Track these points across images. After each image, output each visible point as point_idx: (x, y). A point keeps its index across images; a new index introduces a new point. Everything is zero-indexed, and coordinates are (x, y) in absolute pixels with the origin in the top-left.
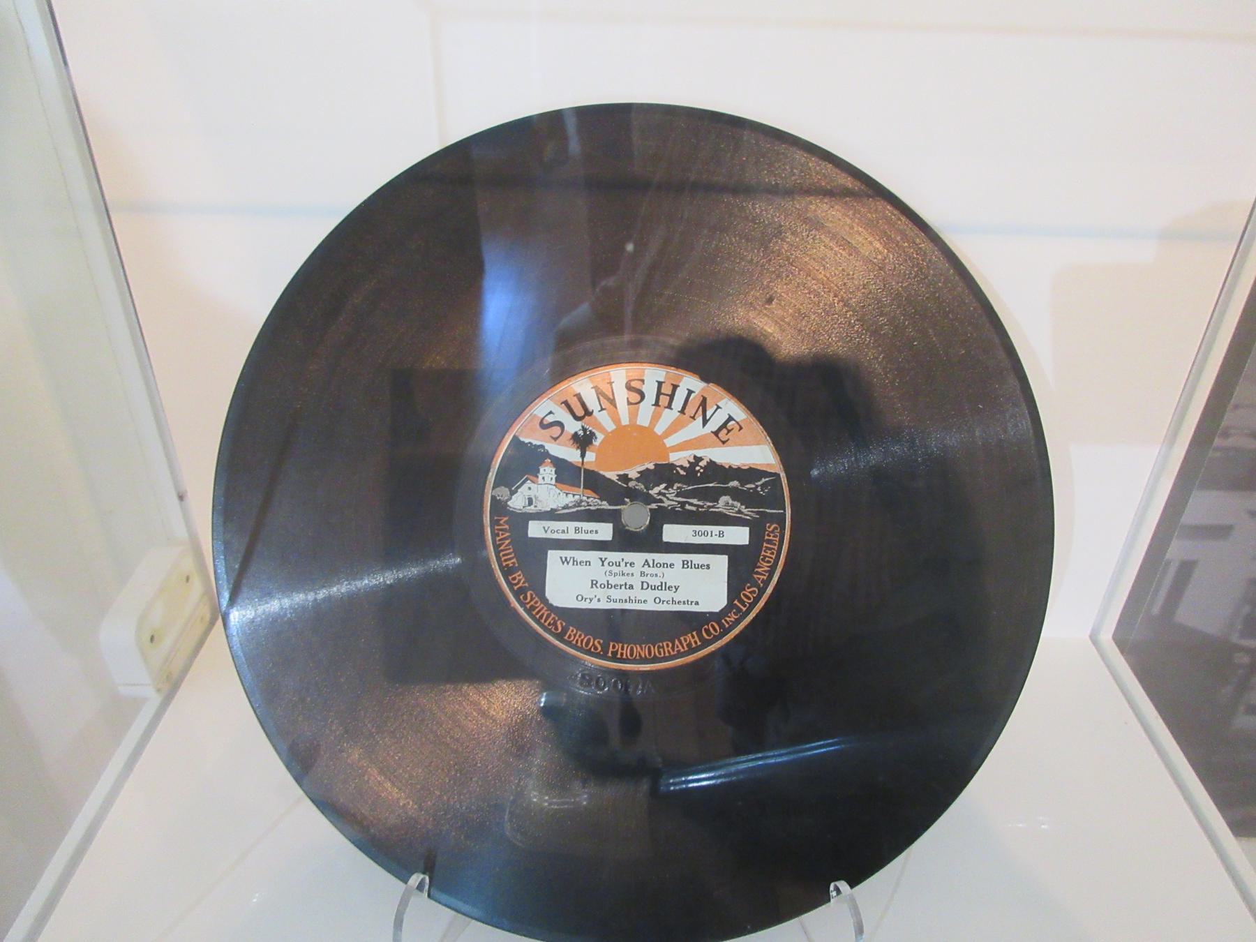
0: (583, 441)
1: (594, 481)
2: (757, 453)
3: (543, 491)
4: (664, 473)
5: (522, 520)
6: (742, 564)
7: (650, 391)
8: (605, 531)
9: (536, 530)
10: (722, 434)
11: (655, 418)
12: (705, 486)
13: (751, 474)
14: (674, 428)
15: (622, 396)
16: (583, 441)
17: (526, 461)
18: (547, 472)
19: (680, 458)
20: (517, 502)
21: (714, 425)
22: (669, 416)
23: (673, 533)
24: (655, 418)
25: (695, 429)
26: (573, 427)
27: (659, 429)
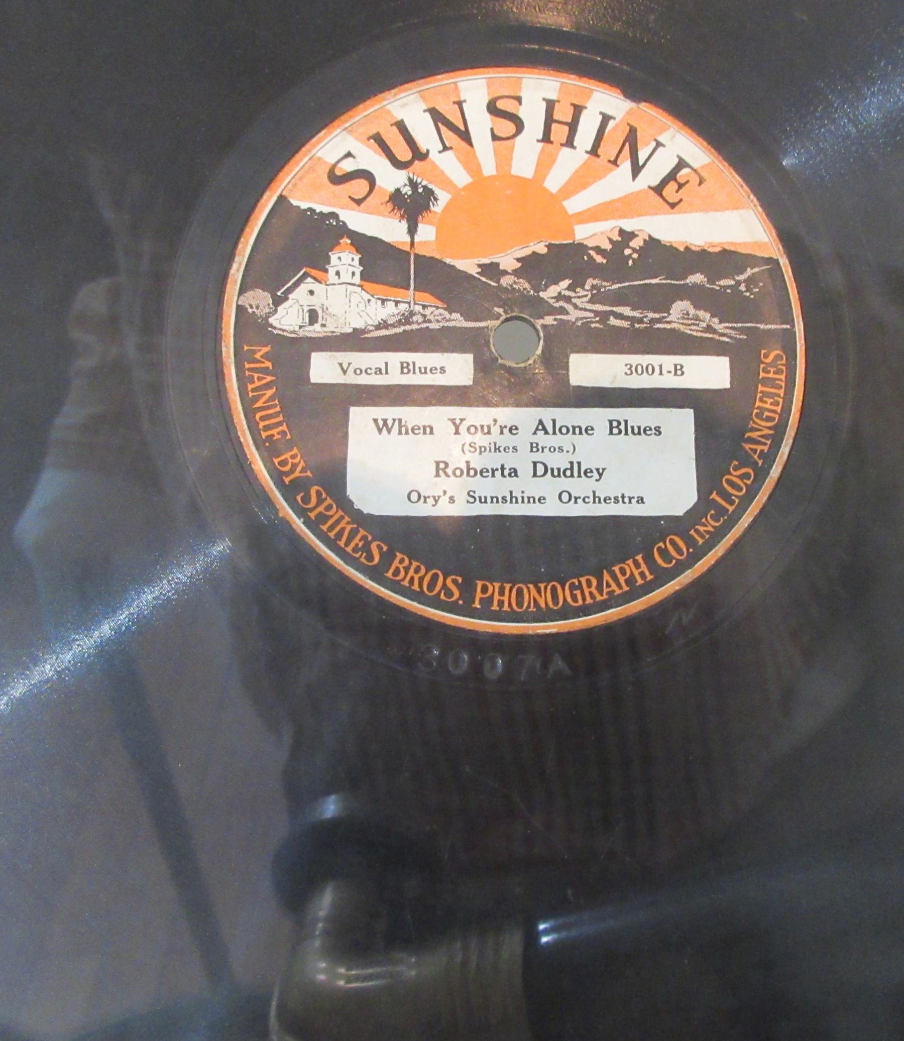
0: (412, 205)
1: (435, 277)
2: (734, 223)
3: (339, 297)
4: (565, 261)
5: (294, 352)
6: (720, 431)
7: (533, 115)
8: (458, 369)
9: (323, 369)
10: (670, 189)
11: (545, 165)
12: (645, 284)
13: (725, 261)
14: (579, 182)
15: (480, 124)
16: (412, 205)
17: (307, 243)
18: (345, 261)
19: (594, 234)
20: (288, 319)
21: (653, 174)
22: (569, 162)
23: (588, 369)
24: (545, 165)
25: (619, 182)
26: (392, 180)
27: (554, 182)
